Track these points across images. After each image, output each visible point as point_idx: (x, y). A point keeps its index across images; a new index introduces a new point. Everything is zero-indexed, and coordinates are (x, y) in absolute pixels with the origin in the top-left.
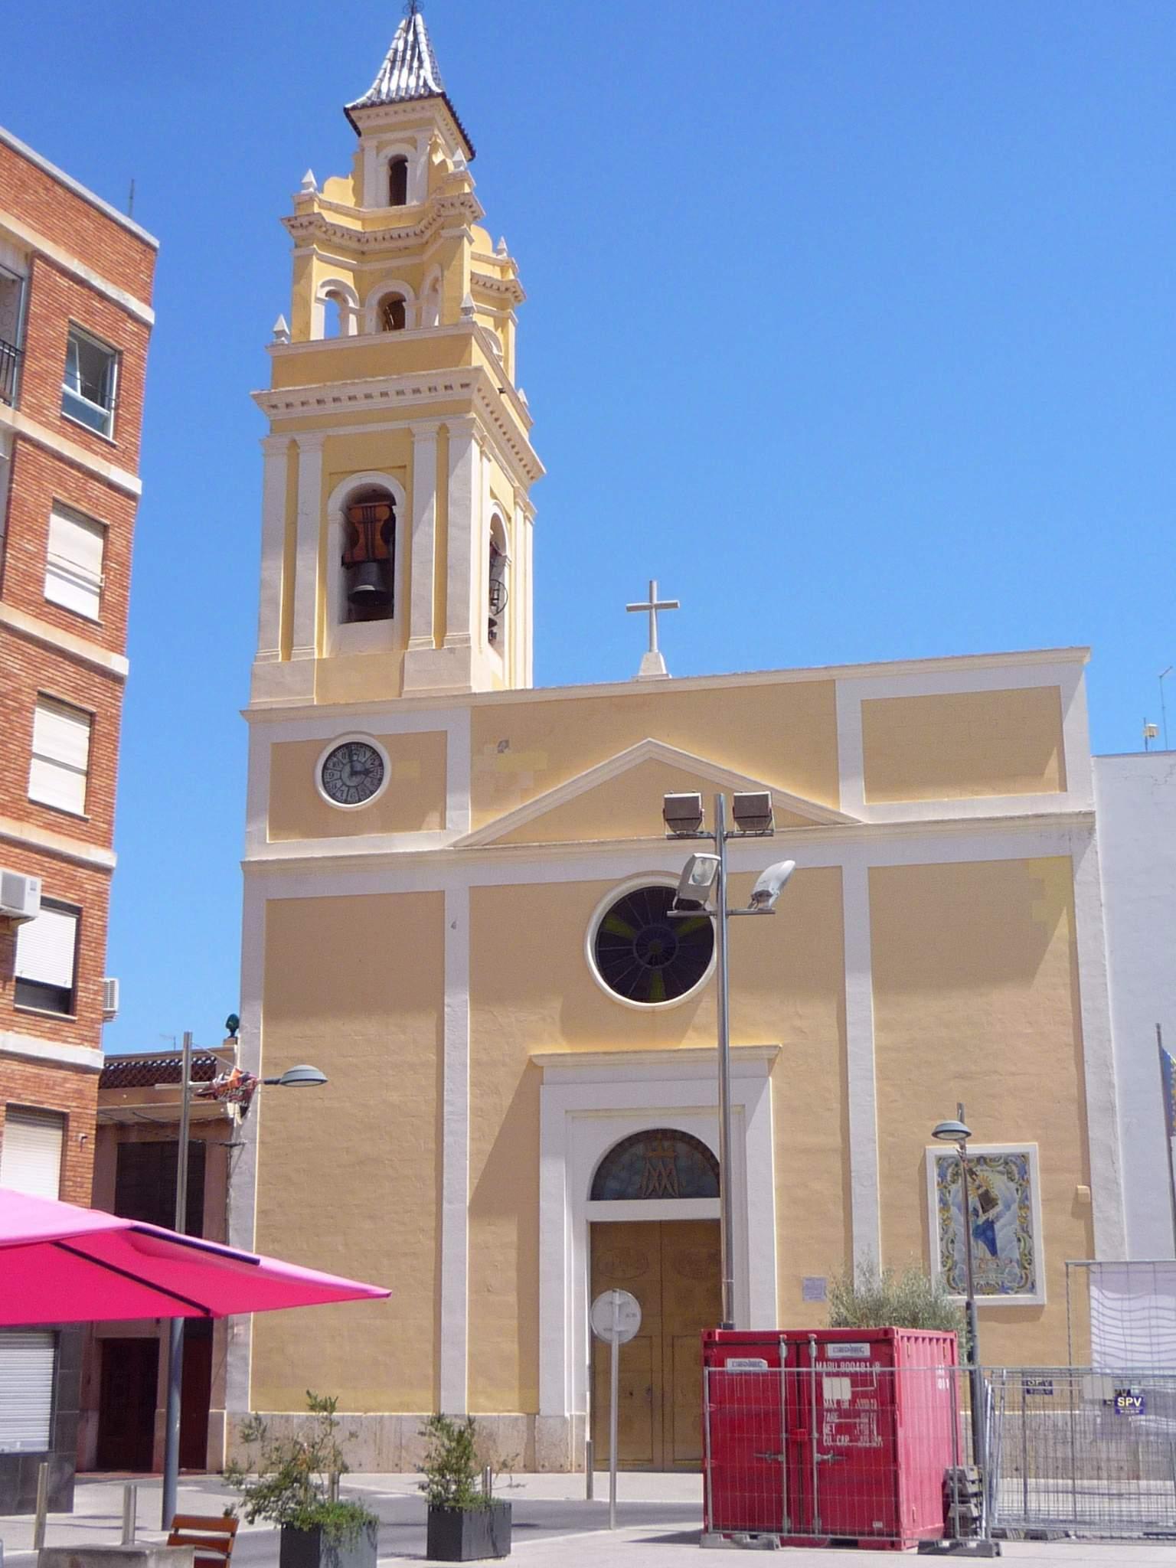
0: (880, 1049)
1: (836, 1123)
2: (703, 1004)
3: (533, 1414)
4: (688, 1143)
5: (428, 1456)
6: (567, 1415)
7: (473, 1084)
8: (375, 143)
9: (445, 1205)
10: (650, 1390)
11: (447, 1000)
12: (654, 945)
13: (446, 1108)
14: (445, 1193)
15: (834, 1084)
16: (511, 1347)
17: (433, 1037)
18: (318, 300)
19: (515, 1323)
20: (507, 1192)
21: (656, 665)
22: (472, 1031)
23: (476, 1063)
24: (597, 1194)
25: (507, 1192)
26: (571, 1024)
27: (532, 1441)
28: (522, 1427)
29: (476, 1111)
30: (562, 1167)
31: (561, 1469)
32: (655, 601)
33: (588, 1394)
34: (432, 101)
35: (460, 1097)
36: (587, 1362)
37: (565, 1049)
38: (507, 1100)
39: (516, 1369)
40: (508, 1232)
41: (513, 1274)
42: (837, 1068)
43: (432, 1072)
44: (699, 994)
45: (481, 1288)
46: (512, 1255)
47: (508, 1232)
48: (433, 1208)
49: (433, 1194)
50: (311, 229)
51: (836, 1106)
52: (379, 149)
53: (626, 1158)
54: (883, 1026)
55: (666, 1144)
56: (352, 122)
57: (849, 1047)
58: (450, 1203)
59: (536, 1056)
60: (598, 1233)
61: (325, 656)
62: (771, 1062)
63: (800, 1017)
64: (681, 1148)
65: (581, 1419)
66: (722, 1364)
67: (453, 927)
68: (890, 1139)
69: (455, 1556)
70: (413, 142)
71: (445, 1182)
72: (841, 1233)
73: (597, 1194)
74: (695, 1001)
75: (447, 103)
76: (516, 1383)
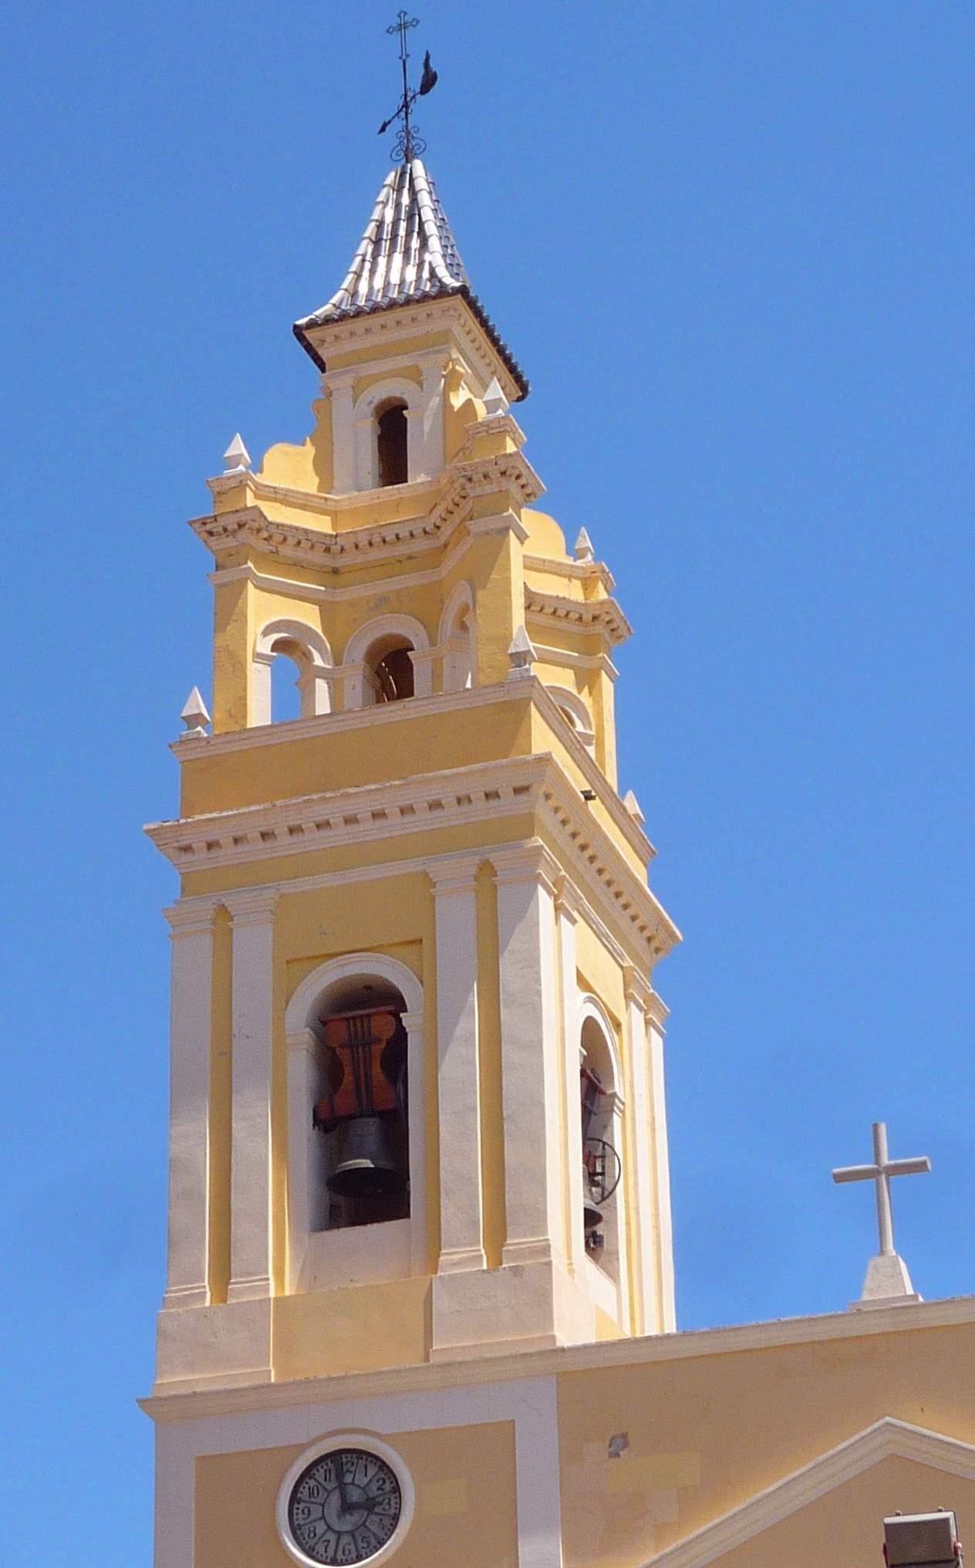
8: (349, 380)
18: (259, 657)
21: (893, 1279)
32: (886, 1161)
34: (446, 302)
50: (243, 535)
52: (356, 392)
56: (309, 348)
61: (287, 1293)
70: (415, 375)
75: (472, 304)
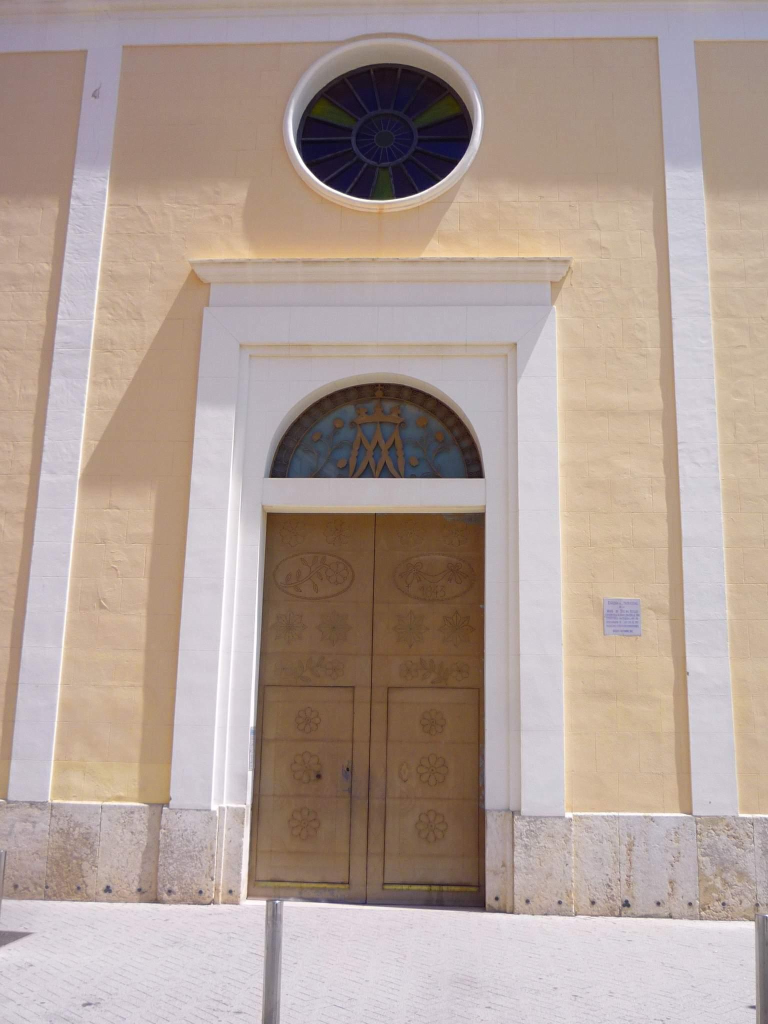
0: (719, 275)
1: (654, 372)
2: (454, 206)
3: (159, 805)
4: (422, 405)
5: (194, 833)
6: (214, 807)
7: (102, 306)
9: (44, 477)
10: (349, 770)
11: (75, 189)
12: (386, 130)
13: (59, 337)
14: (45, 459)
15: (651, 321)
16: (132, 696)
17: (50, 240)
19: (139, 658)
20: (144, 450)
22: (109, 233)
23: (110, 277)
24: (280, 467)
25: (144, 450)
26: (257, 223)
27: (154, 851)
28: (141, 826)
29: (103, 344)
30: (230, 414)
31: (199, 898)
33: (250, 774)
35: (83, 313)
36: (252, 723)
37: (246, 254)
38: (153, 328)
39: (138, 732)
40: (138, 511)
41: (142, 583)
42: (655, 298)
43: (44, 287)
44: (456, 188)
45: (90, 602)
46: (144, 554)
47: (138, 511)
48: (26, 480)
49: (26, 459)
51: (654, 350)
53: (325, 425)
54: (721, 244)
55: (388, 405)
57: (672, 270)
58: (52, 473)
59: (202, 264)
60: (278, 526)
62: (556, 286)
63: (599, 228)
64: (411, 411)
65: (238, 814)
66: (215, 812)
67: (95, 95)
68: (738, 400)
69: (284, 475)
71: (46, 441)
72: (662, 532)
73: (280, 467)
74: (446, 200)
76: (135, 752)
